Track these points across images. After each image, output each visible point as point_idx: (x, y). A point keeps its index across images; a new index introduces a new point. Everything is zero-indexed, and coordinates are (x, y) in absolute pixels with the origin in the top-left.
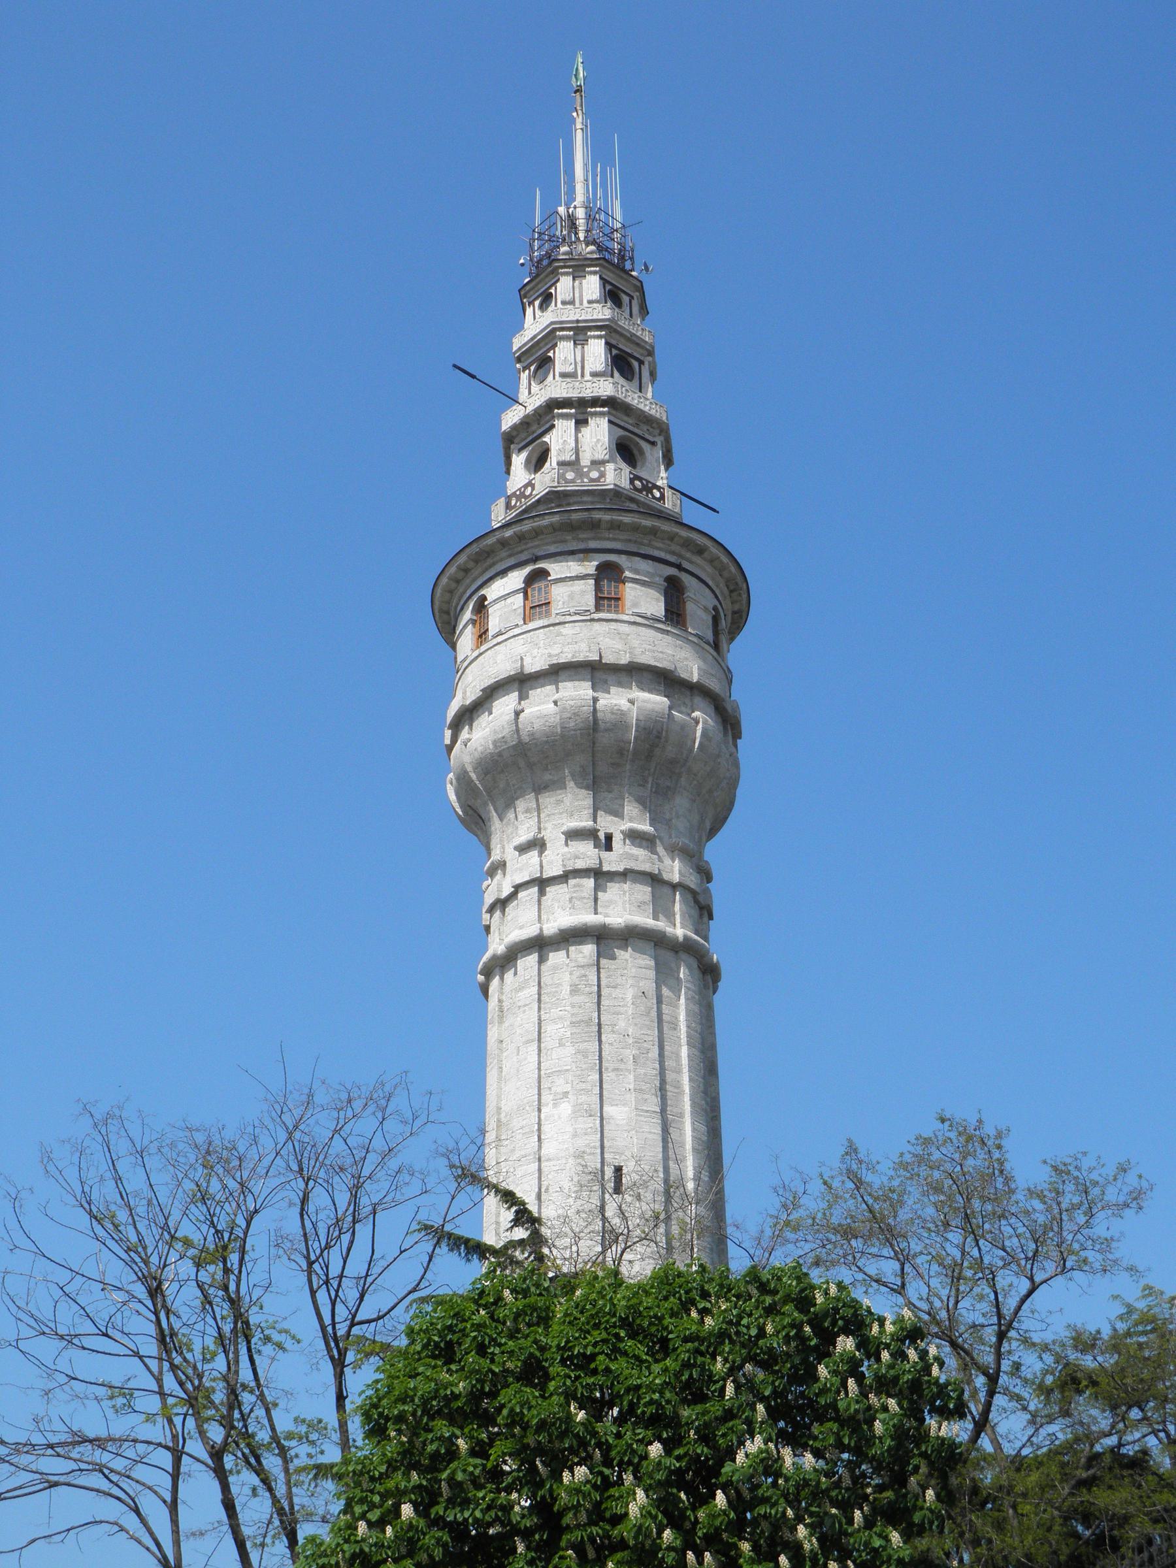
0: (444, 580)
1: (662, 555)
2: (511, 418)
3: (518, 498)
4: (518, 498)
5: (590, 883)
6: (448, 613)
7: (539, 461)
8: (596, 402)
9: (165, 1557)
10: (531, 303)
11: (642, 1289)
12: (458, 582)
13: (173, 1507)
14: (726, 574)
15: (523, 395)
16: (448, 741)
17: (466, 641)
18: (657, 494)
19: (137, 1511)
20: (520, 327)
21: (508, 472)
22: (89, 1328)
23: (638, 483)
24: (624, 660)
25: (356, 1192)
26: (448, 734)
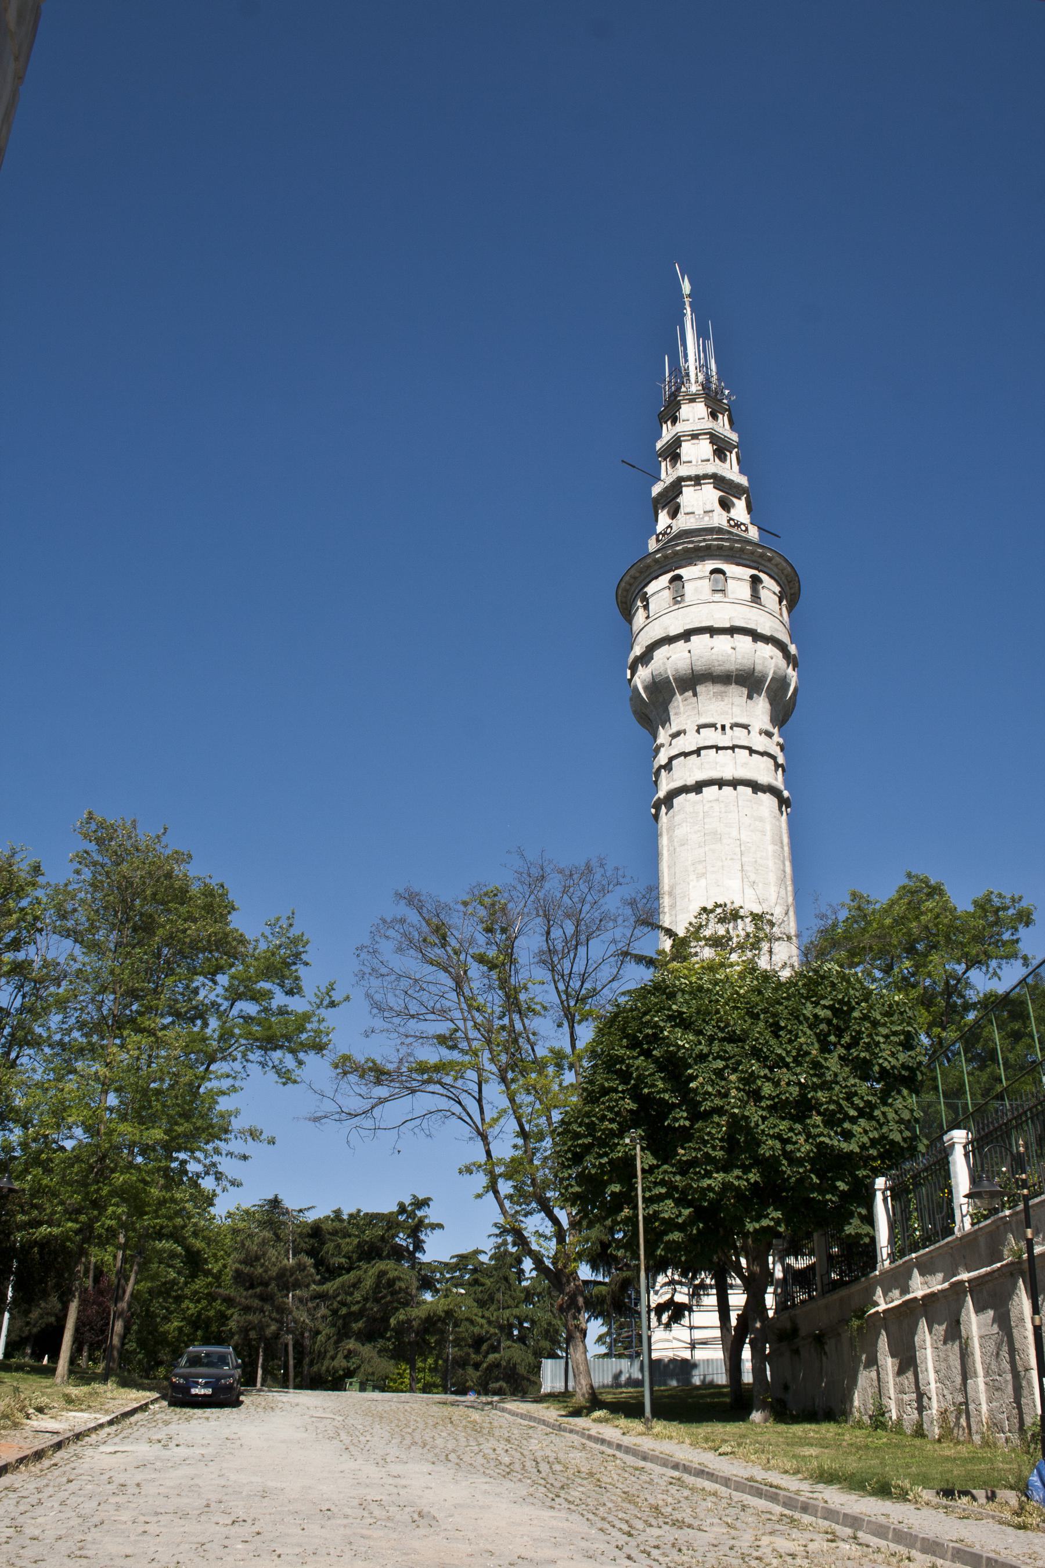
0: (623, 584)
1: (748, 563)
2: (656, 489)
3: (663, 535)
4: (663, 535)
5: (411, 982)
6: (626, 603)
7: (674, 514)
8: (706, 476)
9: (477, 1127)
10: (666, 422)
11: (791, 983)
12: (631, 585)
13: (479, 1101)
14: (785, 572)
15: (663, 475)
16: (629, 677)
17: (640, 617)
18: (743, 528)
19: (460, 1103)
20: (660, 436)
21: (657, 520)
22: (424, 1011)
23: (732, 523)
24: (728, 625)
25: (450, 973)
26: (629, 672)
